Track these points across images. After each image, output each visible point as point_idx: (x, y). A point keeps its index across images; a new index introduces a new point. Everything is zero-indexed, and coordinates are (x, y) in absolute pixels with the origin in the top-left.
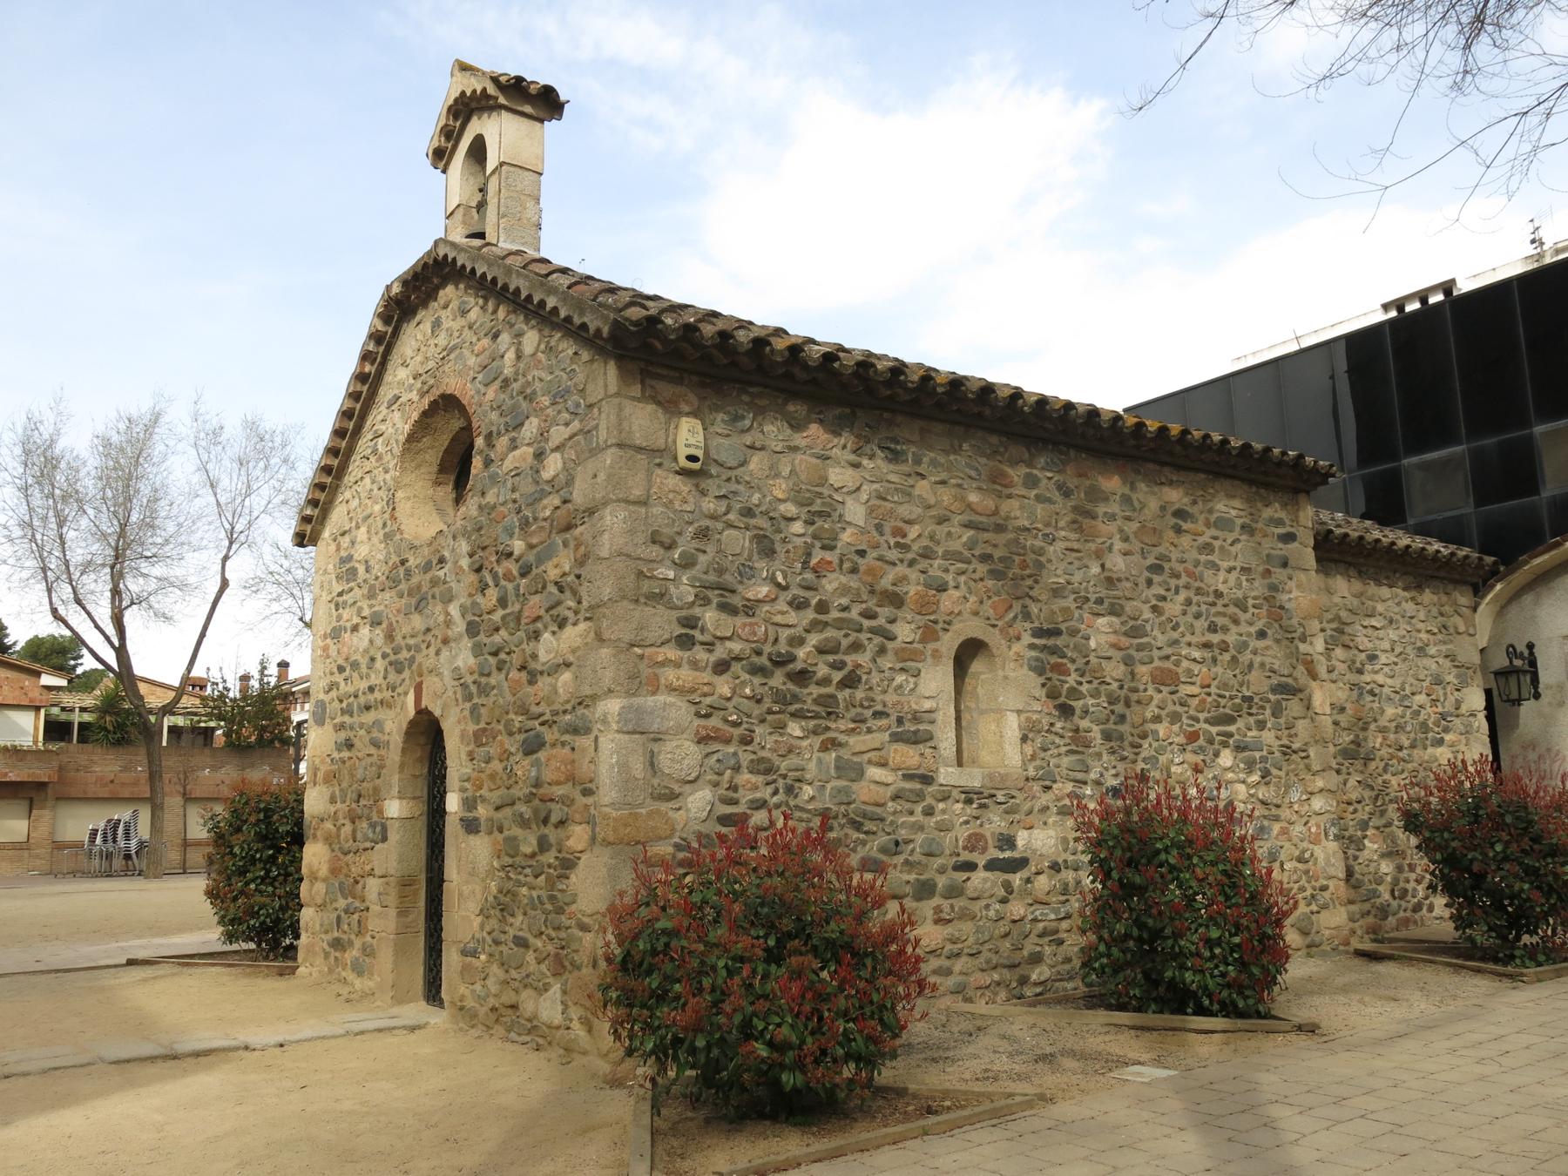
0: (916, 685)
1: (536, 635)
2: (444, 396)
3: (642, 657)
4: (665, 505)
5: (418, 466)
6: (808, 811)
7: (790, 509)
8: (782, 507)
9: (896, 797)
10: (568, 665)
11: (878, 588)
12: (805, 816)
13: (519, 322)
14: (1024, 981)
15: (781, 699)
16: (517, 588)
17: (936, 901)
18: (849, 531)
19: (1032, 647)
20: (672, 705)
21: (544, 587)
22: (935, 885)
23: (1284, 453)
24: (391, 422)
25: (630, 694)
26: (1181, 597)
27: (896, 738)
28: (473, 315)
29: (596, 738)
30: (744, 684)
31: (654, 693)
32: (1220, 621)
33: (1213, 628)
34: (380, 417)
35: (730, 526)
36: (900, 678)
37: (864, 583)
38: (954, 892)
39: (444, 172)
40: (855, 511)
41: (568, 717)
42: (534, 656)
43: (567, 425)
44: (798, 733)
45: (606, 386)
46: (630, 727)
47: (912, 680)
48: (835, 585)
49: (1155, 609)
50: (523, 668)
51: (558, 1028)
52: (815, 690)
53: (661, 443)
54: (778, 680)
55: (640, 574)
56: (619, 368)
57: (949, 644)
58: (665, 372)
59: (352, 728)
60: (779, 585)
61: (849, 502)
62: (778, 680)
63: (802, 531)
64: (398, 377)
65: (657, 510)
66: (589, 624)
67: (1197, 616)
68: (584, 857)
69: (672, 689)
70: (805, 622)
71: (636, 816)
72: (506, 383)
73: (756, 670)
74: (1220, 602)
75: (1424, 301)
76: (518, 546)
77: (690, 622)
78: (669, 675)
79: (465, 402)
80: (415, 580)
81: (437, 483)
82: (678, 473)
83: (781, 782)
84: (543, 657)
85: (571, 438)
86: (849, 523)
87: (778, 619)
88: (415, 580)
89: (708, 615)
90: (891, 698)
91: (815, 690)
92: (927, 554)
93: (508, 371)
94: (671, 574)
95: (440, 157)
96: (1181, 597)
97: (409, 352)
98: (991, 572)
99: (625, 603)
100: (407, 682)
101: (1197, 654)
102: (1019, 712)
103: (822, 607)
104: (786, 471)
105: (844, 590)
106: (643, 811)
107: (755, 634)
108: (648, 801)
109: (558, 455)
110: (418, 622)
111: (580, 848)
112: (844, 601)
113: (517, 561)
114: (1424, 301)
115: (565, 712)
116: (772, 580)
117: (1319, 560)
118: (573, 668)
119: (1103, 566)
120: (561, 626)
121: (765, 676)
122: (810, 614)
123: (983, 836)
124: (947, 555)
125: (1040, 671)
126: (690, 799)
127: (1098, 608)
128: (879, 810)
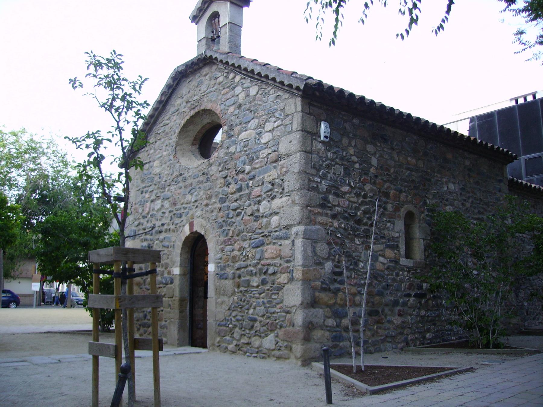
0: (394, 227)
1: (259, 202)
2: (205, 111)
3: (311, 211)
4: (317, 154)
5: (186, 138)
6: (361, 272)
7: (354, 158)
8: (353, 158)
9: (388, 268)
10: (276, 213)
11: (382, 190)
12: (360, 274)
13: (247, 82)
14: (424, 337)
15: (354, 230)
16: (248, 184)
17: (399, 308)
18: (373, 168)
19: (427, 215)
20: (320, 229)
21: (263, 184)
22: (399, 301)
23: (503, 150)
24: (174, 121)
25: (307, 225)
26: (470, 200)
27: (388, 247)
28: (221, 79)
29: (293, 241)
30: (342, 223)
31: (314, 225)
32: (482, 210)
33: (479, 213)
34: (167, 117)
35: (336, 163)
36: (389, 224)
37: (378, 188)
38: (405, 304)
39: (196, 24)
40: (374, 161)
41: (277, 233)
42: (258, 210)
43: (275, 122)
44: (358, 243)
45: (296, 108)
46: (307, 237)
47: (392, 225)
48: (369, 188)
49: (463, 204)
50: (252, 215)
51: (273, 350)
52: (363, 228)
53: (315, 131)
54: (351, 223)
55: (309, 179)
56: (302, 101)
57: (403, 212)
58: (315, 104)
59: (151, 240)
60: (351, 187)
61: (373, 158)
62: (351, 223)
63: (359, 167)
64: (177, 102)
65: (314, 156)
66: (287, 198)
67: (475, 208)
68: (286, 286)
69: (320, 224)
70: (360, 201)
71: (310, 270)
72: (240, 106)
73: (345, 218)
74: (482, 203)
75: (525, 99)
76: (247, 168)
77: (325, 199)
78: (319, 219)
79: (217, 112)
80: (188, 182)
81: (193, 144)
82: (320, 142)
83: (353, 261)
84: (261, 210)
85: (277, 127)
86: (373, 165)
87: (352, 199)
88: (188, 182)
89: (330, 196)
90: (386, 232)
91: (363, 228)
92: (396, 179)
93: (240, 101)
94: (319, 180)
95: (196, 18)
96: (470, 200)
97: (184, 92)
98: (415, 187)
99: (305, 190)
100: (185, 222)
101: (475, 222)
102: (424, 239)
103: (365, 196)
104: (353, 145)
105: (372, 190)
106: (312, 268)
107: (345, 204)
108: (313, 265)
109: (270, 134)
110: (189, 197)
111: (284, 282)
112: (371, 194)
113: (247, 174)
114: (525, 99)
115: (276, 231)
116: (349, 185)
117: (510, 190)
118: (280, 215)
119: (448, 187)
120: (273, 198)
121: (348, 221)
122: (361, 199)
123: (413, 285)
124: (402, 179)
125: (429, 225)
126: (326, 265)
127: (447, 203)
128: (382, 273)
